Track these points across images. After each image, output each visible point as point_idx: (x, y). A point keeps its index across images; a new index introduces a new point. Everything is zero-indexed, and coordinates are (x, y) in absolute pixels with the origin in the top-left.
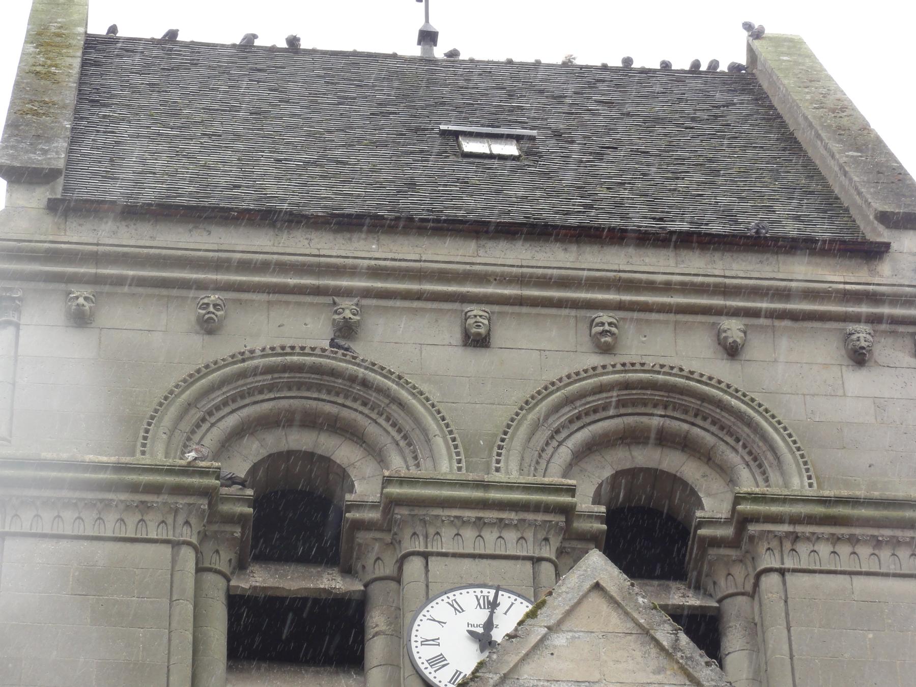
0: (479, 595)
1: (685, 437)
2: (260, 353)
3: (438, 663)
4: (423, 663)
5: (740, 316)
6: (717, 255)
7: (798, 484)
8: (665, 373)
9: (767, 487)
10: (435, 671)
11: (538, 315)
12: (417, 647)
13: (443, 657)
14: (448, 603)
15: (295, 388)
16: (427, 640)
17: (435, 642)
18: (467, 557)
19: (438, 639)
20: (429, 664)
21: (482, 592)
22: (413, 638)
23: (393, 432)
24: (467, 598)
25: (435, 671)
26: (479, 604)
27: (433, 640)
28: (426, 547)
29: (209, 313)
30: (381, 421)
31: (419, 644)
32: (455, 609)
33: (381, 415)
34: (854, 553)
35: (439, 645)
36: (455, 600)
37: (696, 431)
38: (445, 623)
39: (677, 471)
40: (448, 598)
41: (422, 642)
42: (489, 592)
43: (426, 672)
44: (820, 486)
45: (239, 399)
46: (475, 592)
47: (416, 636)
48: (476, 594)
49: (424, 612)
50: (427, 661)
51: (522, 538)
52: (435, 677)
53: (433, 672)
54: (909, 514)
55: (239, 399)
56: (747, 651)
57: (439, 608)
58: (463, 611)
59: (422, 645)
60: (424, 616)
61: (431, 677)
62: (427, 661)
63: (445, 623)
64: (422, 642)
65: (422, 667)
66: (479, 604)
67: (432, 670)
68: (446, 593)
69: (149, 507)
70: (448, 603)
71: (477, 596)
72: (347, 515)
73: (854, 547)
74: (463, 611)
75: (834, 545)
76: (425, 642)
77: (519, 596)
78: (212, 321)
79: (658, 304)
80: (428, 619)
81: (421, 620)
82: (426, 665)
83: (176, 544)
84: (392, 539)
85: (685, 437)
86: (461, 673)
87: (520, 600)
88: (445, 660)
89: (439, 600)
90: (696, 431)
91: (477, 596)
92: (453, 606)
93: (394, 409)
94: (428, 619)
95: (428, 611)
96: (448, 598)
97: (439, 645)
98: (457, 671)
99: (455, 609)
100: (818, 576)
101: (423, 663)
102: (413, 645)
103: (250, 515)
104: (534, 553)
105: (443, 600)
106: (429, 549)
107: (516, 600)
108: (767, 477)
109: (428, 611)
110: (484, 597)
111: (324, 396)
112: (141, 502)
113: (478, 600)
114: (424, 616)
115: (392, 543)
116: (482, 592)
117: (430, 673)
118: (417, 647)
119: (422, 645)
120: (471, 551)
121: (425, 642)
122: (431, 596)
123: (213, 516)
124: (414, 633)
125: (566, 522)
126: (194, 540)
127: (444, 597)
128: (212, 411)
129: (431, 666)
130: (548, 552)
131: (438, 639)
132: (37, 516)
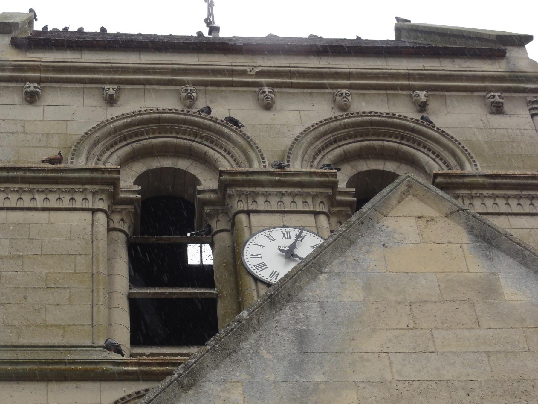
0: (284, 231)
3: (261, 267)
4: (252, 267)
6: (202, 54)
8: (185, 114)
10: (260, 271)
11: (222, 91)
12: (247, 259)
13: (264, 264)
14: (265, 236)
16: (253, 255)
17: (259, 256)
18: (63, 210)
19: (261, 254)
20: (256, 267)
21: (285, 230)
22: (245, 254)
23: (431, 155)
24: (277, 233)
25: (260, 271)
26: (284, 236)
27: (257, 255)
28: (248, 208)
31: (249, 257)
32: (270, 239)
34: (484, 204)
35: (261, 258)
36: (269, 234)
38: (264, 246)
39: (192, 164)
40: (265, 233)
41: (250, 256)
42: (290, 230)
43: (254, 272)
45: (209, 141)
46: (281, 230)
47: (247, 253)
48: (282, 231)
49: (251, 240)
50: (254, 266)
51: (85, 199)
52: (260, 274)
53: (258, 272)
54: (4, 174)
55: (209, 141)
57: (260, 238)
58: (275, 240)
59: (250, 258)
60: (251, 242)
61: (258, 274)
62: (254, 266)
63: (264, 246)
64: (250, 256)
65: (252, 269)
66: (284, 236)
67: (258, 271)
68: (264, 231)
69: (50, 191)
70: (265, 236)
71: (283, 232)
73: (72, 195)
74: (275, 240)
75: (495, 199)
76: (252, 256)
77: (308, 231)
79: (88, 79)
80: (253, 244)
81: (249, 245)
82: (254, 268)
83: (316, 214)
86: (276, 272)
87: (309, 233)
88: (266, 265)
89: (259, 234)
91: (283, 232)
92: (268, 237)
93: (223, 141)
94: (253, 244)
95: (253, 240)
96: (265, 233)
97: (261, 258)
98: (274, 271)
99: (270, 239)
100: (52, 213)
101: (252, 267)
102: (245, 258)
104: (82, 205)
105: (262, 234)
106: (250, 209)
107: (307, 233)
108: (238, 162)
109: (253, 240)
110: (287, 232)
111: (151, 136)
112: (6, 188)
113: (284, 234)
114: (251, 242)
116: (285, 230)
117: (257, 272)
118: (247, 259)
119: (250, 258)
120: (67, 206)
121: (252, 256)
122: (253, 232)
124: (245, 251)
125: (114, 189)
126: (106, 208)
127: (263, 233)
129: (257, 269)
130: (102, 205)
131: (261, 254)
132: (72, 199)
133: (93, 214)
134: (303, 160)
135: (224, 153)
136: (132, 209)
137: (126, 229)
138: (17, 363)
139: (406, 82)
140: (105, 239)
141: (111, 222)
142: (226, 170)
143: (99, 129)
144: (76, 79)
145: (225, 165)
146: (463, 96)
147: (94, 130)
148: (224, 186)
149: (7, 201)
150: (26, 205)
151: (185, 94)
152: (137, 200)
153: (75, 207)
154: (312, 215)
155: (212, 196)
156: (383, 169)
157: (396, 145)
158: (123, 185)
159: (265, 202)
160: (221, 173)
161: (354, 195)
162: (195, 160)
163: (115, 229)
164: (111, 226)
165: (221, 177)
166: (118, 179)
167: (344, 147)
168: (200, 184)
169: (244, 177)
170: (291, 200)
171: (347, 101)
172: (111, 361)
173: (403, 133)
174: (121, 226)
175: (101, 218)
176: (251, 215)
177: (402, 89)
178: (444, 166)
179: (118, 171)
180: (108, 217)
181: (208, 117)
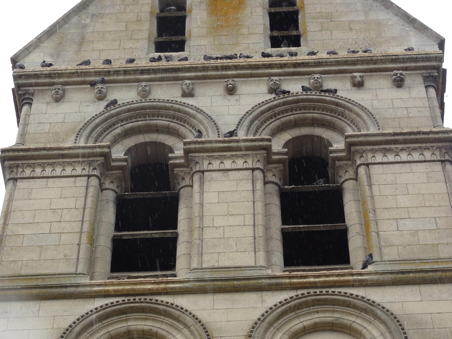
1: (168, 126)
2: (166, 101)
5: (272, 29)
7: (373, 130)
9: (359, 132)
11: (248, 81)
15: (129, 119)
29: (143, 88)
30: (185, 125)
33: (185, 123)
37: (172, 124)
44: (383, 130)
56: (349, 226)
72: (331, 155)
78: (370, 51)
84: (352, 163)
85: (168, 126)
90: (172, 124)
103: (287, 158)
115: (352, 165)
123: (268, 160)
128: (98, 137)
133: (253, 172)
134: (248, 129)
135: (349, 122)
136: (121, 173)
137: (278, 182)
138: (403, 272)
139: (234, 72)
140: (262, 189)
141: (266, 178)
142: (28, 148)
143: (97, 118)
144: (416, 67)
145: (350, 132)
146: (296, 79)
147: (93, 119)
148: (349, 145)
149: (84, 171)
150: (28, 175)
151: (313, 80)
152: (285, 159)
153: (433, 159)
154: (440, 163)
155: (343, 154)
156: (144, 141)
157: (167, 123)
158: (114, 156)
159: (408, 155)
160: (347, 137)
161: (286, 154)
162: (327, 129)
163: (106, 189)
164: (267, 180)
165: (346, 140)
166: (271, 146)
167: (282, 120)
168: (332, 146)
169: (201, 146)
170: (231, 161)
171: (318, 83)
172: (150, 281)
173: (175, 114)
174: (274, 179)
175: (259, 174)
176: (205, 173)
177: (133, 82)
178: (356, 129)
179: (270, 140)
180: (100, 180)
181: (117, 106)
